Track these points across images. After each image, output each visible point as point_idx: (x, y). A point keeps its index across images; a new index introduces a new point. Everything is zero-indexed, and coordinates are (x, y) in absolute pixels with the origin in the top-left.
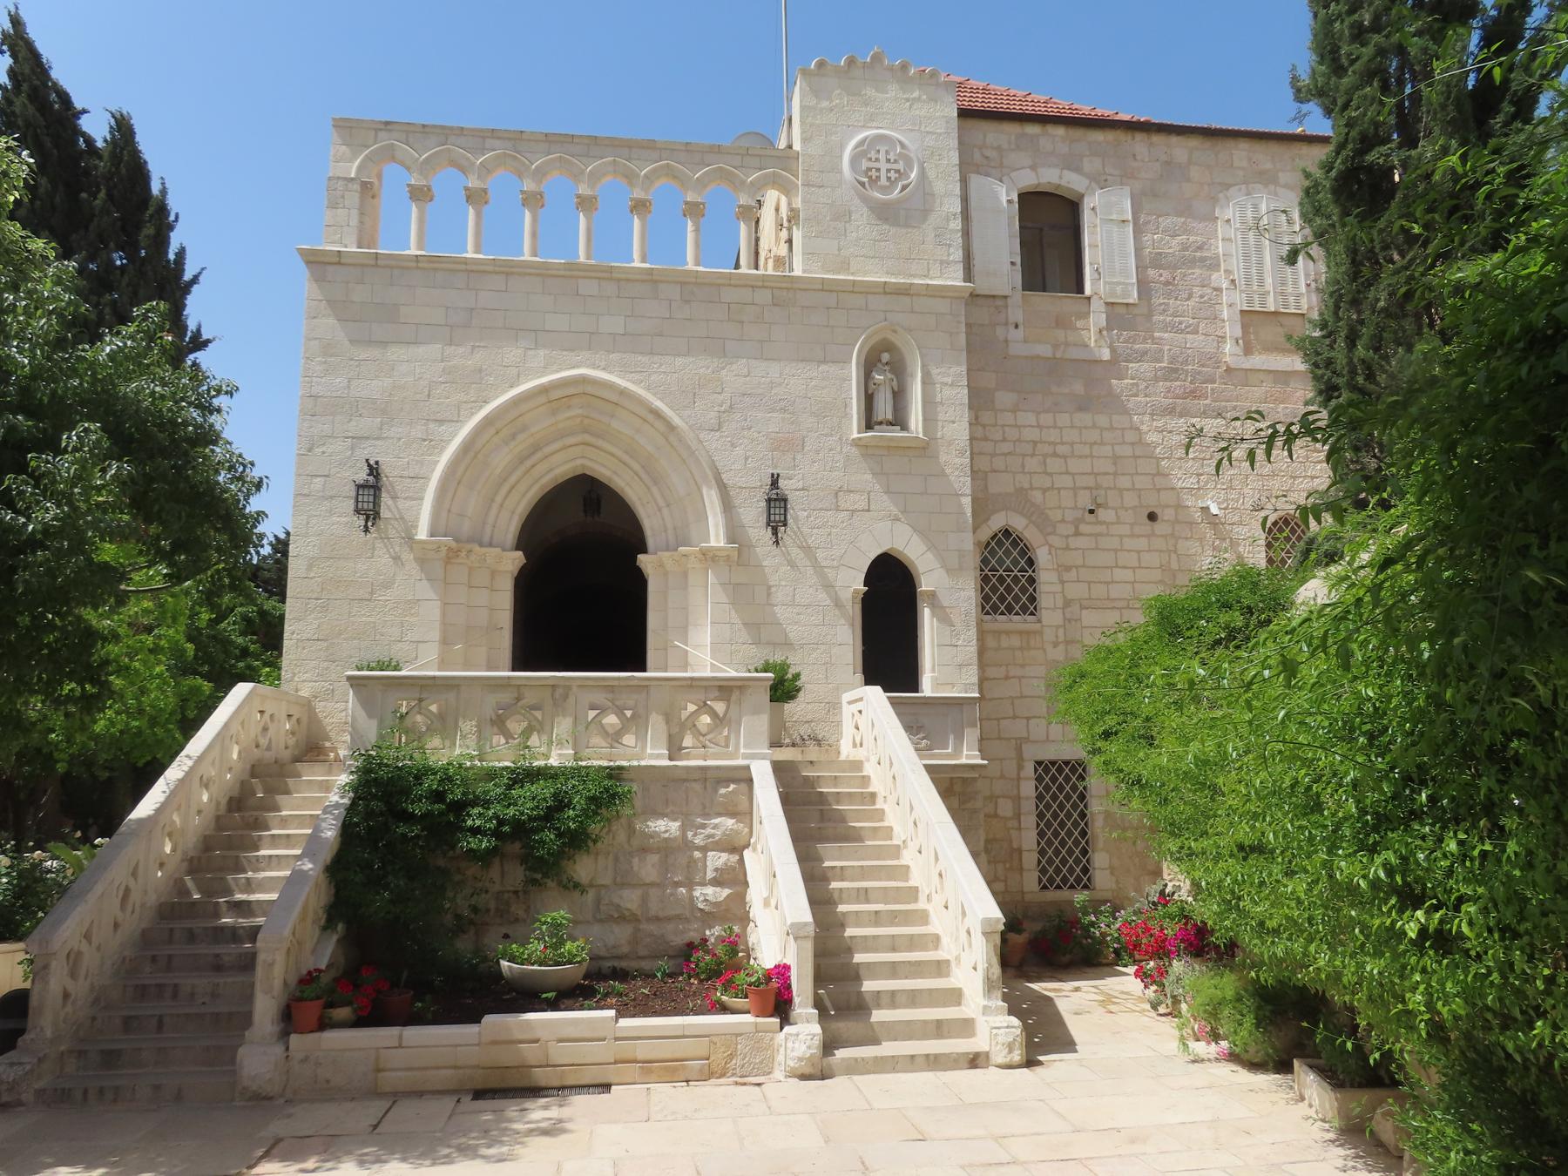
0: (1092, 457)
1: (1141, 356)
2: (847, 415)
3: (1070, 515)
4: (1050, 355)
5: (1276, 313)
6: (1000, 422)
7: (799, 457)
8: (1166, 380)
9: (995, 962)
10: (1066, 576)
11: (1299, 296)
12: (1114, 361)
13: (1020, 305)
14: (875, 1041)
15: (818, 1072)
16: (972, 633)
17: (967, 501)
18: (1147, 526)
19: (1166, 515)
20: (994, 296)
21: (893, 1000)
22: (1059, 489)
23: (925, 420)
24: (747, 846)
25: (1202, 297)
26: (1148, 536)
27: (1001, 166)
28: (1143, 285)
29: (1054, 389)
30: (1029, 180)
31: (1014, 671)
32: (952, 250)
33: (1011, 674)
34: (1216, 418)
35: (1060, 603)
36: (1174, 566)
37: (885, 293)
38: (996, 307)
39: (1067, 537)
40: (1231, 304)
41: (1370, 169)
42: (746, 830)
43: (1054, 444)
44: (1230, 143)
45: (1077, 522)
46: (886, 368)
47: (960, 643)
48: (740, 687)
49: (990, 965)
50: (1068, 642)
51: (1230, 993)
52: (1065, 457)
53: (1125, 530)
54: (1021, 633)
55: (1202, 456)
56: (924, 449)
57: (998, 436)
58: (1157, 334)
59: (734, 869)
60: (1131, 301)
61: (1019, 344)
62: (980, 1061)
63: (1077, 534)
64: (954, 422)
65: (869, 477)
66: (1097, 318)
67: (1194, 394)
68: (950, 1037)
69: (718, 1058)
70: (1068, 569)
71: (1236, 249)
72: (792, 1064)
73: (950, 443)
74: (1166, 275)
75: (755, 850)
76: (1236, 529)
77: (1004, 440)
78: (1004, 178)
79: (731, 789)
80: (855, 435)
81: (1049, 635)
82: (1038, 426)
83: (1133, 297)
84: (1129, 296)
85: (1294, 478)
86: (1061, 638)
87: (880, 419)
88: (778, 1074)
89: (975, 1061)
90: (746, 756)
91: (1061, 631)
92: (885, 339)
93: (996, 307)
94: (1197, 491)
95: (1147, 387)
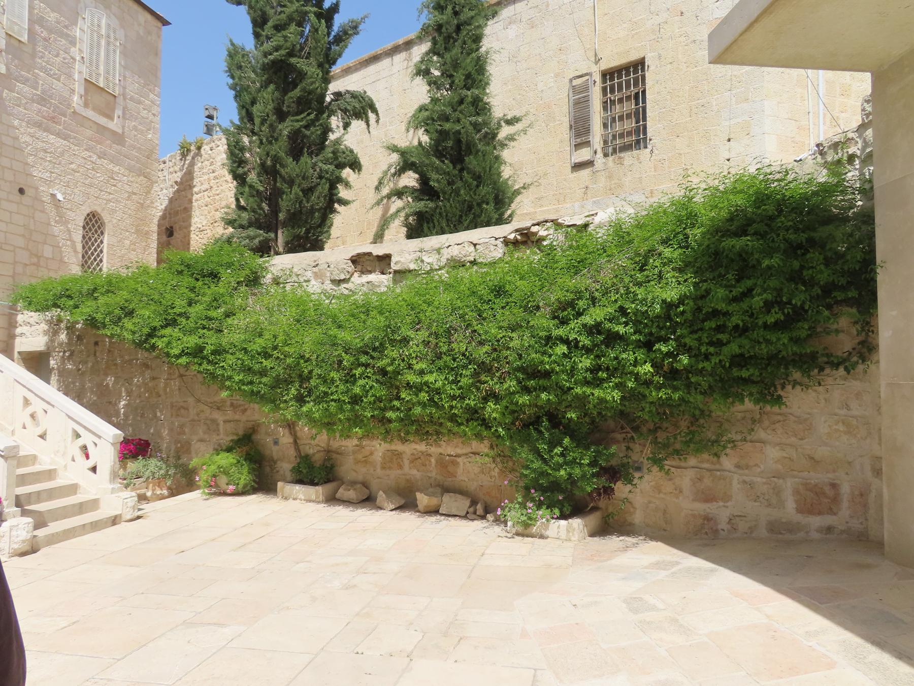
1: (25, 81)
8: (38, 104)
9: (117, 460)
11: (114, 84)
18: (17, 197)
19: (29, 192)
25: (64, 59)
28: (31, 32)
34: (65, 140)
40: (80, 72)
49: (115, 462)
55: (54, 161)
60: (22, 40)
67: (52, 119)
71: (86, 38)
72: (16, 546)
76: (69, 213)
83: (25, 38)
84: (22, 36)
85: (101, 191)
89: (115, 521)
94: (49, 183)
95: (26, 103)
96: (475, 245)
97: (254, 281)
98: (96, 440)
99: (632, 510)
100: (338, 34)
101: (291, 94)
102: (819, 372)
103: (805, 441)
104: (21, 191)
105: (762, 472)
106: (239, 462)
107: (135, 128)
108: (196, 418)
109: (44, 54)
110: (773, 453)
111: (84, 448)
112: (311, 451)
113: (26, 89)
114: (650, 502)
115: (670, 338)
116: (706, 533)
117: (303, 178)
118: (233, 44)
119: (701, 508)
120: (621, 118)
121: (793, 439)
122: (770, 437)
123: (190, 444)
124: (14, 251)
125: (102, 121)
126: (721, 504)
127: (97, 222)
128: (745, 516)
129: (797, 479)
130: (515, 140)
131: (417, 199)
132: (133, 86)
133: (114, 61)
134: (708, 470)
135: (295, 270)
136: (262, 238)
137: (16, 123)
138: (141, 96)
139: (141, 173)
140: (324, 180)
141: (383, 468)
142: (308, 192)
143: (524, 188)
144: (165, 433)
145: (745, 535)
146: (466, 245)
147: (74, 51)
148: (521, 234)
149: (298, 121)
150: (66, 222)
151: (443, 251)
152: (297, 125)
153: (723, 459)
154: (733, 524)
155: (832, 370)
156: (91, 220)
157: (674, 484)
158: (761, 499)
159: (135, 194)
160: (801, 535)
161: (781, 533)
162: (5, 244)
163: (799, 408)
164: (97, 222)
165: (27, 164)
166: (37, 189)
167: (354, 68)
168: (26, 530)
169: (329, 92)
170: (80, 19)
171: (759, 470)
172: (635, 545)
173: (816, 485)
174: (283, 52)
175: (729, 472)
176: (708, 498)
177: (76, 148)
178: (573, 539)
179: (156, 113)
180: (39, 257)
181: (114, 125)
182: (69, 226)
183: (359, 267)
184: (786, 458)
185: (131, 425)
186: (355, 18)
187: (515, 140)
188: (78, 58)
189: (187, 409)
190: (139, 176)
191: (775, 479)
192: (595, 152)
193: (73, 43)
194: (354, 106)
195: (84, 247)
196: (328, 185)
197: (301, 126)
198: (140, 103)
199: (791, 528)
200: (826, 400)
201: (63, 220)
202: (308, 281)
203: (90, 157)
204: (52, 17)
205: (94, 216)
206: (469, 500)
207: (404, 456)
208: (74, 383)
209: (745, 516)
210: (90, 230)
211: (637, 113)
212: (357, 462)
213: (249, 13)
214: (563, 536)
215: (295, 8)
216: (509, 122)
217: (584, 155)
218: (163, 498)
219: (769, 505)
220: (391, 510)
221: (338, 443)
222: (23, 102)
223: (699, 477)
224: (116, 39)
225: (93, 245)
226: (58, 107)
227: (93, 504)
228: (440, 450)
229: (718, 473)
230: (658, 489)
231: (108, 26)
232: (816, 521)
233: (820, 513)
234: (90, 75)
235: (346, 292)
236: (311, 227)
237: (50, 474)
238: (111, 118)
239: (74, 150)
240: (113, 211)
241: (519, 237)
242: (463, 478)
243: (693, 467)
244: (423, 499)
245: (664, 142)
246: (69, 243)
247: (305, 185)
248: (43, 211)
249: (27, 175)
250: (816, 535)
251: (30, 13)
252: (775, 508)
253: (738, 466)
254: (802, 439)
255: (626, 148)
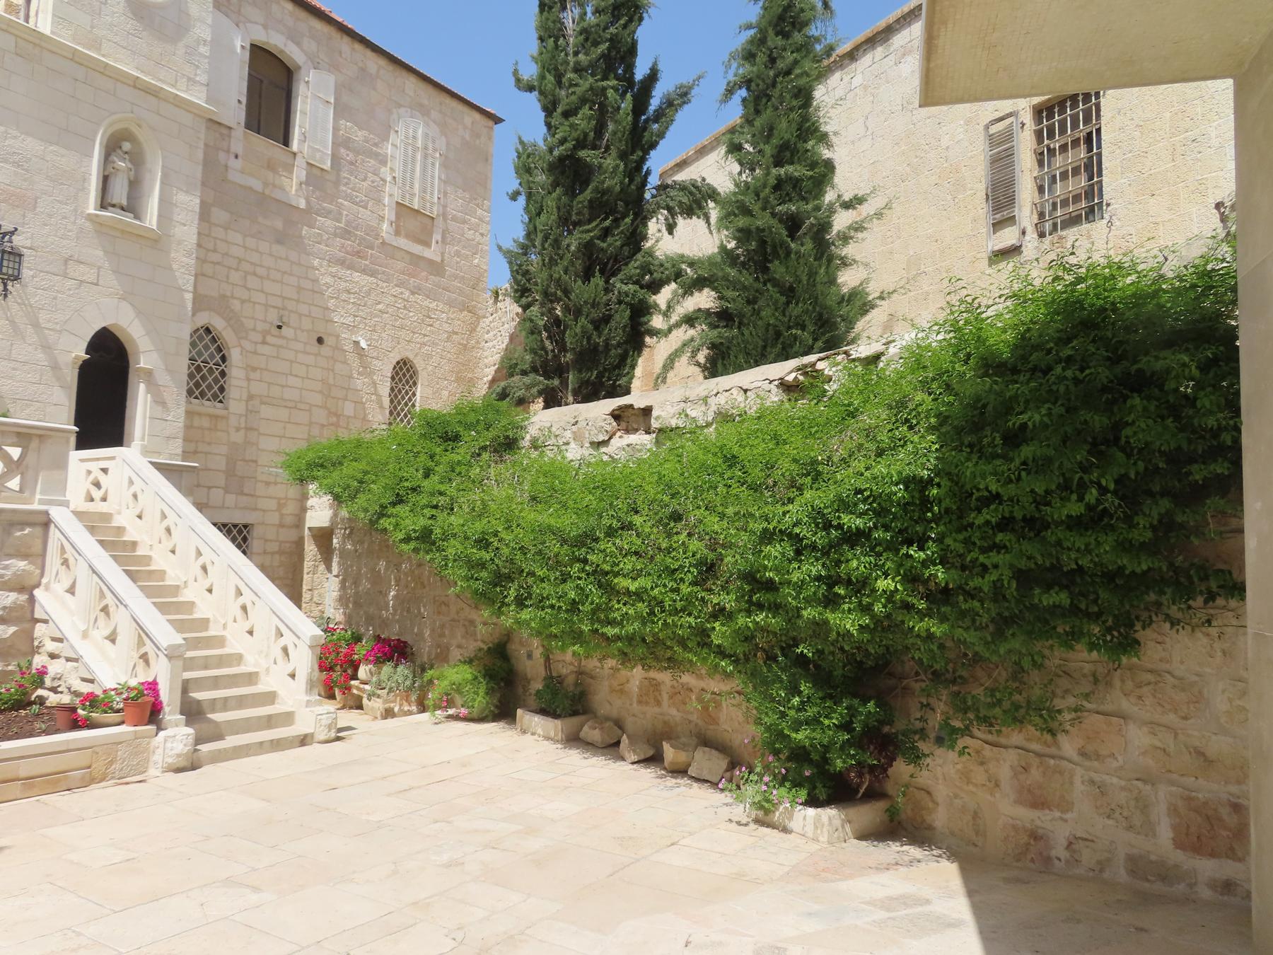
0: (282, 282)
1: (327, 214)
2: (84, 189)
3: (260, 326)
4: (261, 191)
5: (417, 211)
6: (213, 235)
7: (30, 215)
9: (316, 667)
10: (253, 375)
11: (432, 203)
12: (308, 210)
13: (242, 139)
14: (220, 737)
15: (191, 765)
16: (181, 411)
17: (189, 297)
18: (315, 348)
19: (329, 341)
20: (219, 124)
21: (225, 704)
22: (254, 303)
23: (160, 216)
24: (38, 585)
25: (373, 182)
26: (316, 355)
27: (239, 12)
28: (335, 158)
29: (260, 219)
30: (261, 37)
31: (202, 447)
32: (198, 72)
33: (199, 449)
34: (371, 276)
35: (245, 396)
36: (331, 381)
37: (135, 87)
38: (221, 134)
39: (256, 343)
40: (391, 195)
41: (579, 160)
42: (38, 571)
43: (255, 264)
44: (404, 73)
45: (265, 333)
46: (126, 156)
47: (169, 418)
48: (40, 436)
50: (248, 429)
51: (469, 677)
52: (261, 277)
53: (300, 346)
54: (211, 416)
56: (156, 241)
57: (211, 246)
58: (340, 200)
59: (22, 607)
60: (325, 168)
61: (238, 173)
62: (308, 740)
63: (264, 343)
64: (185, 225)
65: (100, 253)
66: (299, 173)
67: (358, 254)
68: (276, 727)
69: (98, 767)
70: (254, 369)
71: (399, 154)
72: (170, 760)
73: (179, 243)
74: (351, 157)
75: (47, 588)
77: (215, 251)
78: (240, 25)
79: (26, 532)
80: (91, 210)
81: (233, 421)
82: (245, 247)
83: (327, 165)
84: (325, 164)
86: (243, 425)
87: (114, 202)
88: (153, 771)
89: (304, 741)
90: (41, 502)
91: (243, 419)
92: (126, 129)
93: (221, 134)
94: (352, 328)
96: (746, 391)
97: (509, 445)
98: (297, 641)
99: (931, 805)
100: (660, 107)
101: (580, 198)
102: (1206, 602)
103: (1189, 722)
104: (320, 340)
105: (1121, 768)
106: (476, 678)
107: (458, 254)
108: (456, 617)
109: (349, 179)
110: (1138, 737)
111: (285, 650)
112: (564, 671)
113: (329, 222)
114: (956, 796)
115: (930, 537)
116: (1032, 860)
117: (593, 306)
118: (521, 142)
119: (1026, 815)
120: (1064, 176)
121: (1172, 716)
122: (1136, 709)
123: (448, 649)
124: (310, 410)
125: (417, 249)
126: (1058, 814)
127: (408, 370)
128: (1093, 841)
129: (1174, 789)
130: (865, 229)
131: (713, 326)
132: (456, 203)
133: (433, 177)
134: (1038, 755)
135: (554, 429)
136: (541, 387)
137: (316, 262)
138: (466, 214)
139: (465, 307)
140: (623, 306)
141: (640, 702)
142: (601, 323)
143: (881, 298)
144: (427, 633)
145: (1091, 874)
146: (734, 391)
147: (385, 172)
148: (805, 374)
149: (589, 231)
150: (371, 373)
151: (712, 401)
152: (587, 237)
153: (1061, 738)
154: (1074, 851)
155: (1227, 599)
156: (401, 369)
157: (986, 771)
158: (1117, 815)
159: (456, 333)
160: (1181, 888)
161: (1148, 880)
162: (301, 402)
163: (1182, 663)
164: (408, 370)
165: (327, 309)
166: (338, 336)
167: (709, 147)
168: (184, 742)
169: (649, 186)
170: (392, 132)
171: (1115, 764)
172: (913, 862)
173: (1206, 803)
174: (569, 145)
175: (1070, 761)
176: (1039, 803)
177: (385, 285)
178: (821, 839)
179: (485, 232)
180: (338, 416)
181: (431, 253)
182: (375, 377)
183: (624, 425)
184: (1160, 748)
185: (398, 621)
186: (685, 82)
187: (865, 229)
188: (389, 179)
189: (447, 605)
190: (461, 311)
191: (1139, 784)
192: (1024, 233)
193: (384, 162)
194: (680, 202)
195: (392, 401)
196: (628, 312)
197: (592, 238)
198: (464, 222)
199: (1165, 873)
200: (1224, 652)
201: (367, 370)
202: (567, 444)
203: (402, 293)
204: (359, 135)
205: (405, 364)
206: (726, 761)
207: (662, 687)
208: (352, 566)
209: (1093, 841)
210: (400, 380)
211: (1089, 167)
212: (612, 691)
213: (539, 100)
214: (810, 834)
215: (588, 86)
216: (847, 205)
217: (1008, 237)
218: (410, 713)
219: (1130, 828)
220: (633, 763)
221: (592, 664)
222: (324, 238)
223: (1024, 764)
224: (435, 150)
225: (403, 398)
226: (364, 239)
227: (288, 718)
228: (702, 684)
229: (1052, 762)
230: (966, 776)
231: (426, 135)
232: (1207, 868)
233: (1213, 855)
234: (403, 197)
235: (605, 458)
236: (605, 370)
237: (251, 678)
238: (427, 244)
239: (382, 288)
240: (429, 356)
241: (801, 378)
242: (726, 727)
243: (1017, 747)
244: (669, 752)
245: (1130, 206)
246: (374, 397)
247: (595, 314)
248: (345, 362)
249: (327, 321)
250: (1206, 893)
251: (334, 135)
252: (1139, 833)
253: (1083, 753)
254: (1185, 718)
255: (1073, 221)
